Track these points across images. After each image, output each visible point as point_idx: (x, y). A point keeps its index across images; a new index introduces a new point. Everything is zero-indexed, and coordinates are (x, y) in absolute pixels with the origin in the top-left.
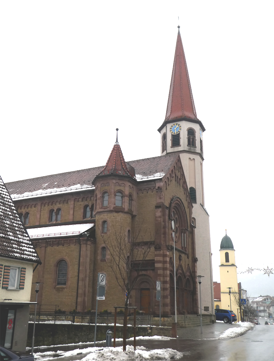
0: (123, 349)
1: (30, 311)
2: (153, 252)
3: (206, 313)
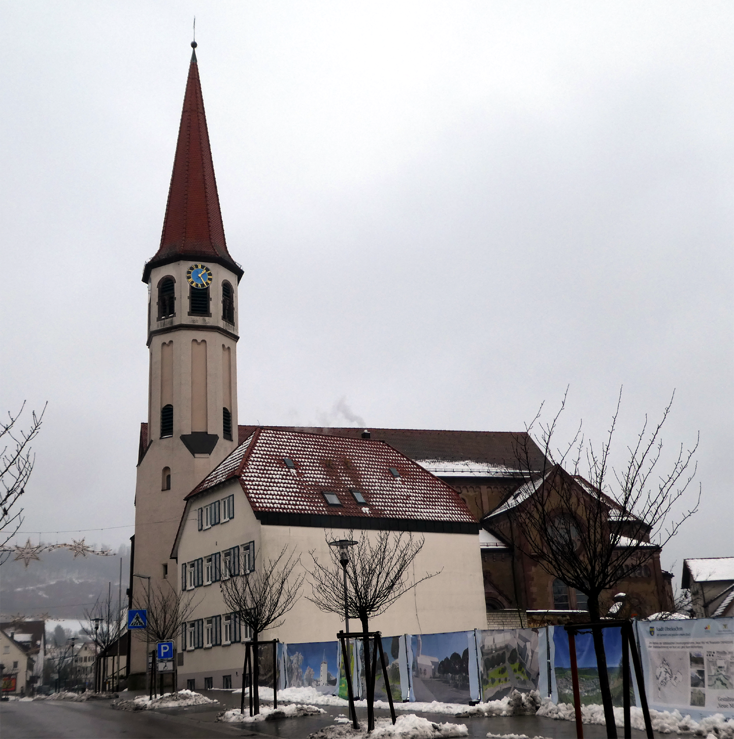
1: (468, 492)
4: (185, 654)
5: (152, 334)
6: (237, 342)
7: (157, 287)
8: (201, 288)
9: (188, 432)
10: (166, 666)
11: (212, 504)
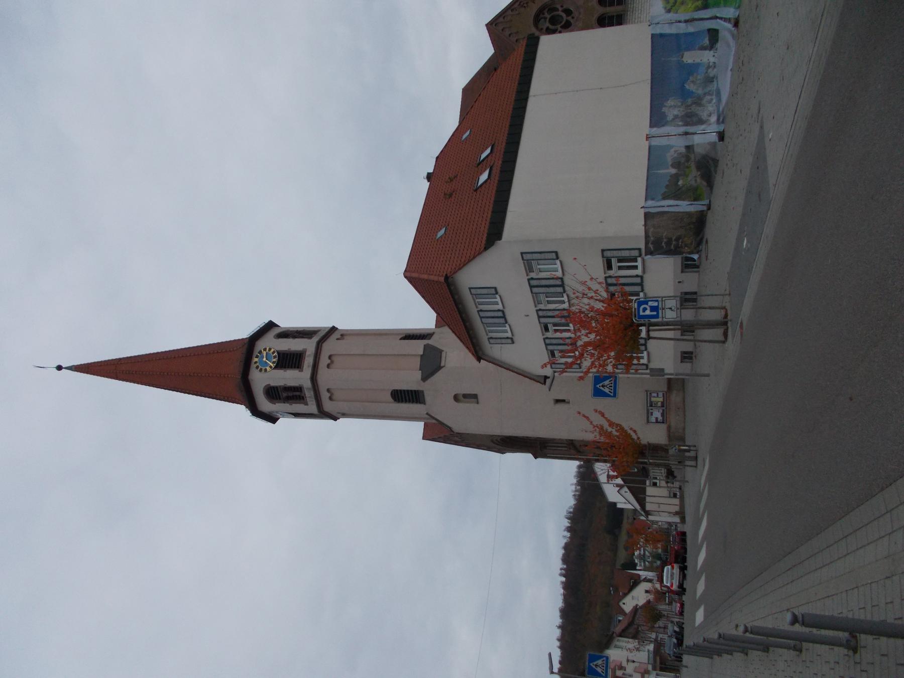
0: (695, 62)
2: (654, 471)
3: (688, 315)
4: (651, 366)
5: (323, 414)
6: (337, 328)
7: (275, 404)
8: (277, 359)
9: (418, 375)
10: (670, 308)
11: (482, 322)
